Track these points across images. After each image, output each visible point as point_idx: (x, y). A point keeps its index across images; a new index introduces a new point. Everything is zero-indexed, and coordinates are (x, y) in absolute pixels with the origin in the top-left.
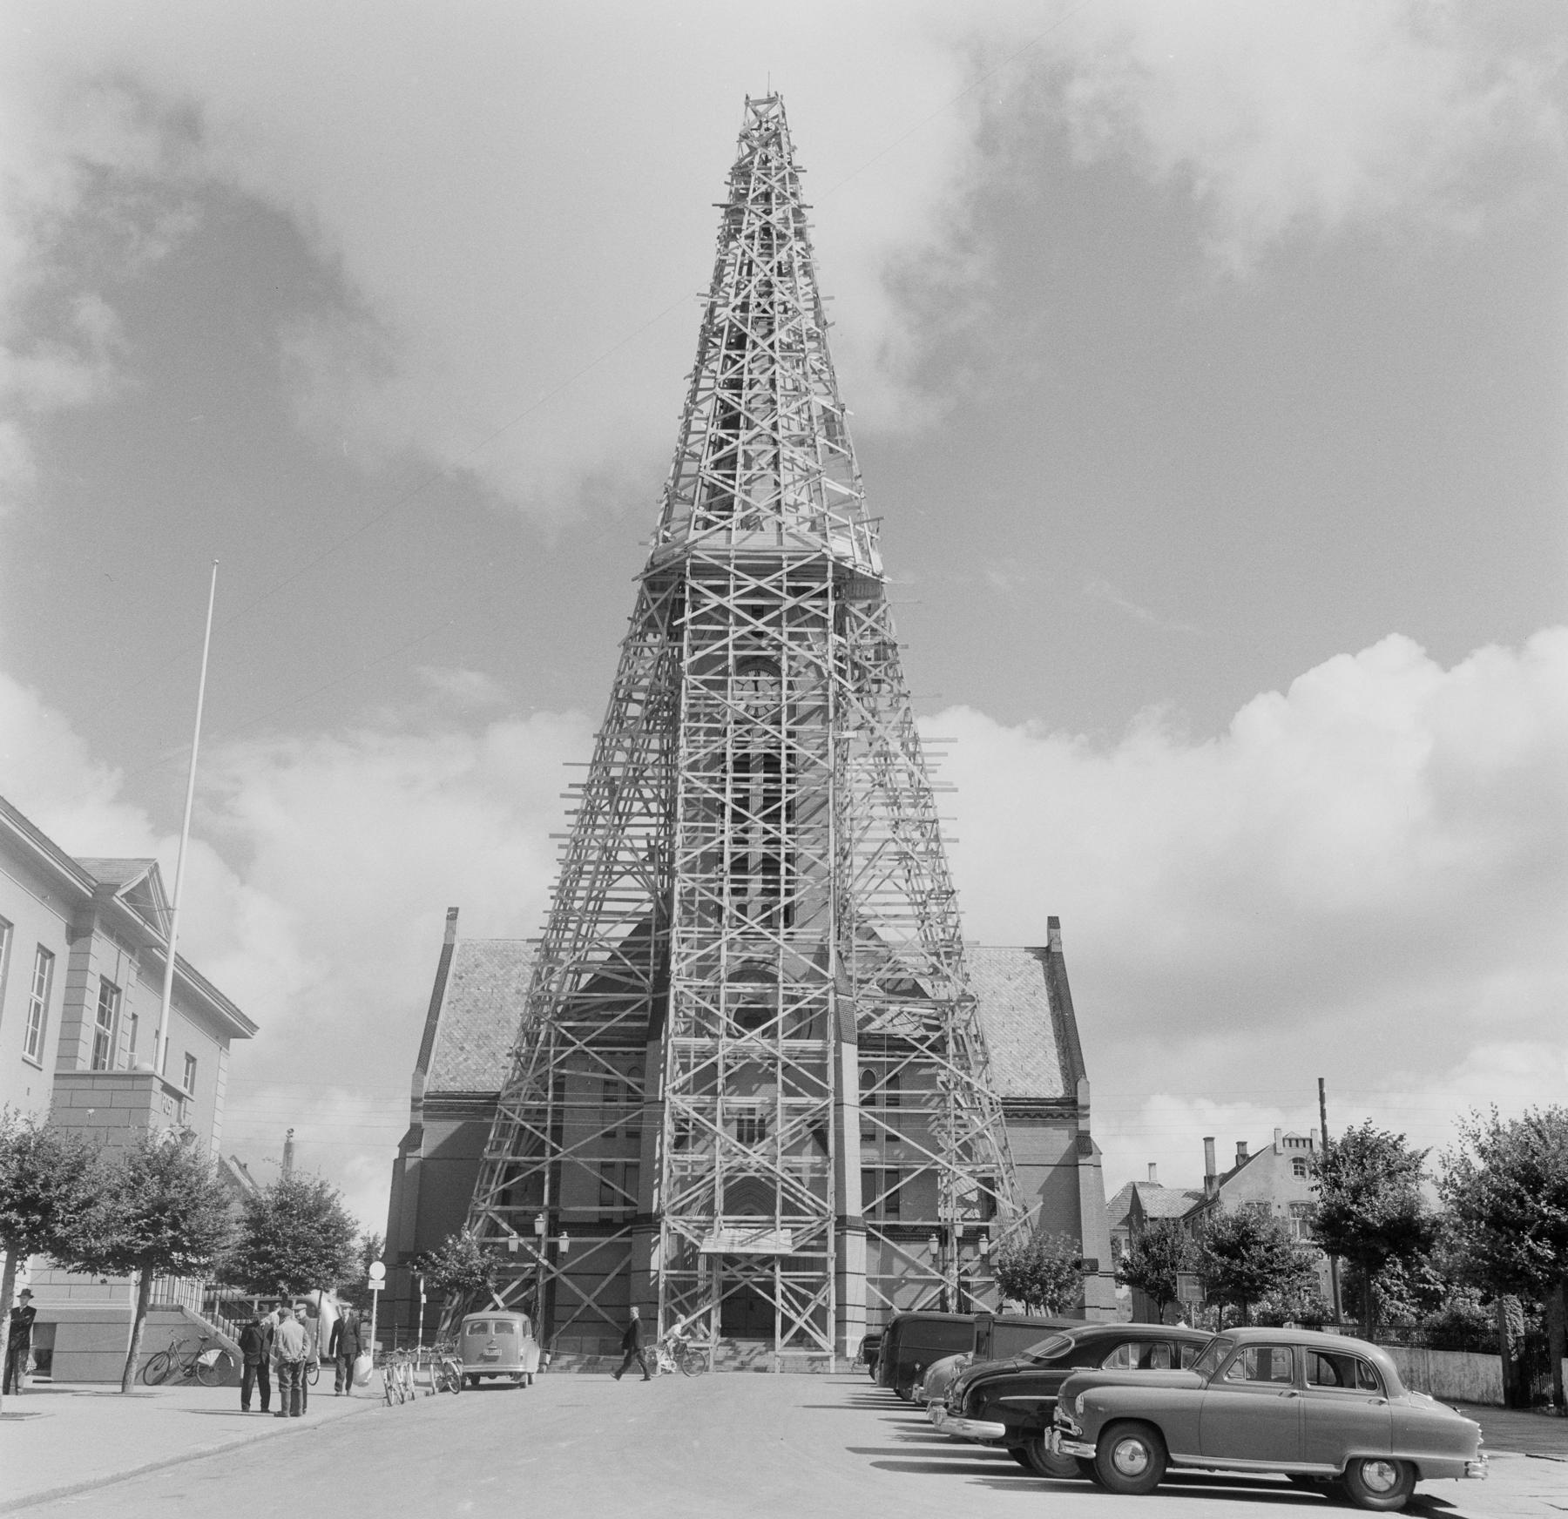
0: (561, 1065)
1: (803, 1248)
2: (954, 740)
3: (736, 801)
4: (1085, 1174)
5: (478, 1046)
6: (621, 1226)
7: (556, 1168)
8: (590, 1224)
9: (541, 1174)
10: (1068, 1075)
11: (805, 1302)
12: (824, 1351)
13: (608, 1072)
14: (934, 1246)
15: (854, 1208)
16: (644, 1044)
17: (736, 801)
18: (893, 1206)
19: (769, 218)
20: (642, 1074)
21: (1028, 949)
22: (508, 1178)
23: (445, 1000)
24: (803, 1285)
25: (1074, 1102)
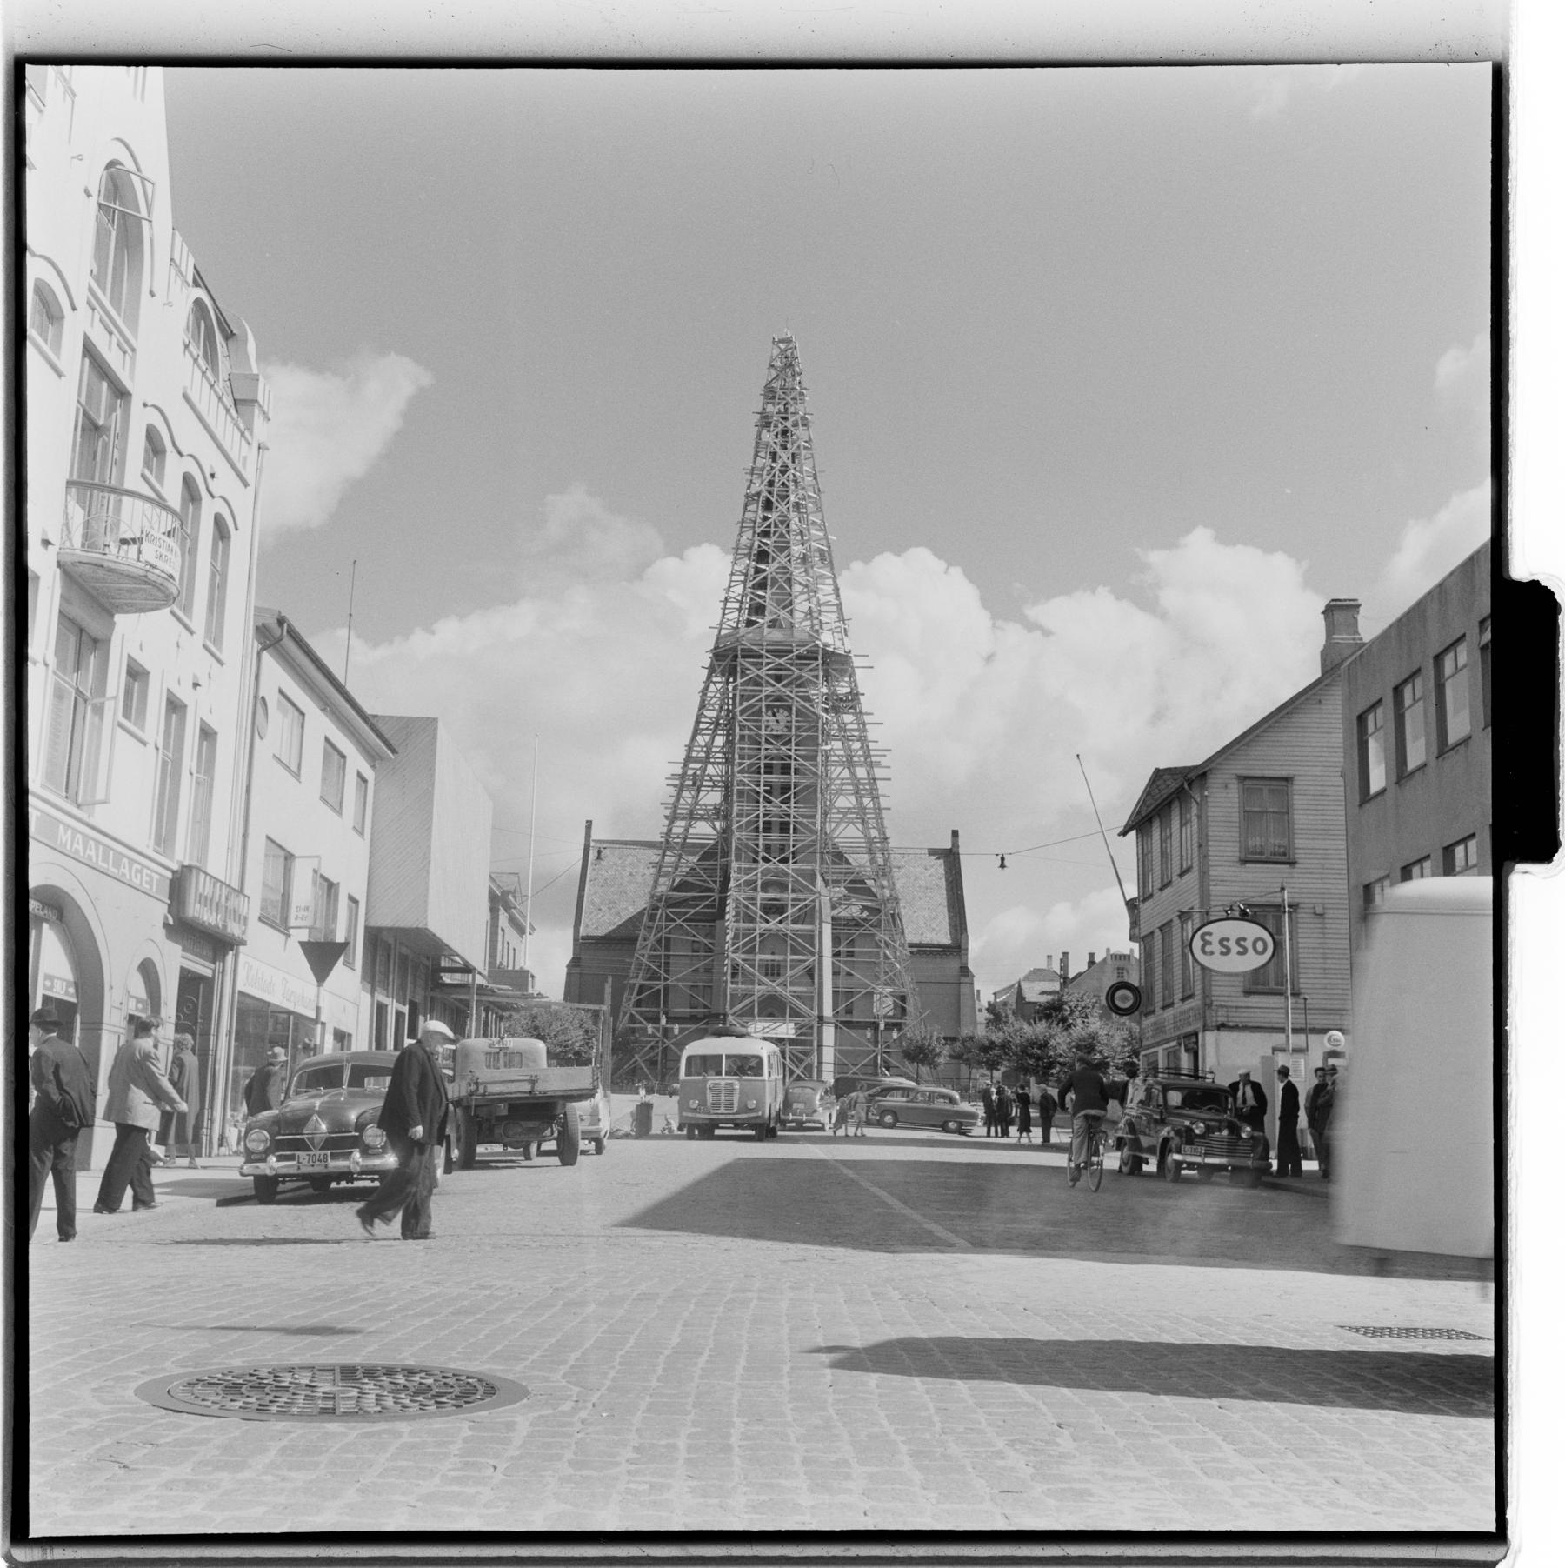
0: (670, 932)
1: (801, 1034)
2: (890, 750)
3: (765, 791)
4: (964, 989)
5: (609, 908)
6: (702, 1019)
7: (666, 988)
8: (685, 1018)
9: (659, 990)
10: (955, 925)
11: (801, 1061)
12: (59, 358)
13: (694, 936)
14: (869, 1034)
15: (828, 1011)
16: (714, 921)
17: (765, 791)
18: (849, 1011)
19: (786, 424)
20: (713, 937)
21: (932, 852)
22: (639, 993)
23: (588, 879)
24: (801, 1052)
25: (960, 947)
